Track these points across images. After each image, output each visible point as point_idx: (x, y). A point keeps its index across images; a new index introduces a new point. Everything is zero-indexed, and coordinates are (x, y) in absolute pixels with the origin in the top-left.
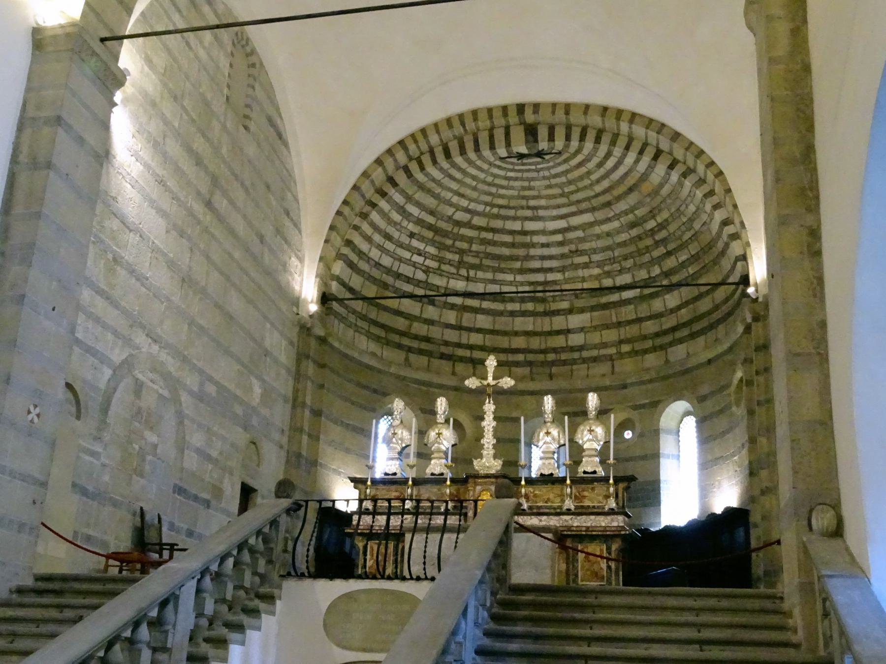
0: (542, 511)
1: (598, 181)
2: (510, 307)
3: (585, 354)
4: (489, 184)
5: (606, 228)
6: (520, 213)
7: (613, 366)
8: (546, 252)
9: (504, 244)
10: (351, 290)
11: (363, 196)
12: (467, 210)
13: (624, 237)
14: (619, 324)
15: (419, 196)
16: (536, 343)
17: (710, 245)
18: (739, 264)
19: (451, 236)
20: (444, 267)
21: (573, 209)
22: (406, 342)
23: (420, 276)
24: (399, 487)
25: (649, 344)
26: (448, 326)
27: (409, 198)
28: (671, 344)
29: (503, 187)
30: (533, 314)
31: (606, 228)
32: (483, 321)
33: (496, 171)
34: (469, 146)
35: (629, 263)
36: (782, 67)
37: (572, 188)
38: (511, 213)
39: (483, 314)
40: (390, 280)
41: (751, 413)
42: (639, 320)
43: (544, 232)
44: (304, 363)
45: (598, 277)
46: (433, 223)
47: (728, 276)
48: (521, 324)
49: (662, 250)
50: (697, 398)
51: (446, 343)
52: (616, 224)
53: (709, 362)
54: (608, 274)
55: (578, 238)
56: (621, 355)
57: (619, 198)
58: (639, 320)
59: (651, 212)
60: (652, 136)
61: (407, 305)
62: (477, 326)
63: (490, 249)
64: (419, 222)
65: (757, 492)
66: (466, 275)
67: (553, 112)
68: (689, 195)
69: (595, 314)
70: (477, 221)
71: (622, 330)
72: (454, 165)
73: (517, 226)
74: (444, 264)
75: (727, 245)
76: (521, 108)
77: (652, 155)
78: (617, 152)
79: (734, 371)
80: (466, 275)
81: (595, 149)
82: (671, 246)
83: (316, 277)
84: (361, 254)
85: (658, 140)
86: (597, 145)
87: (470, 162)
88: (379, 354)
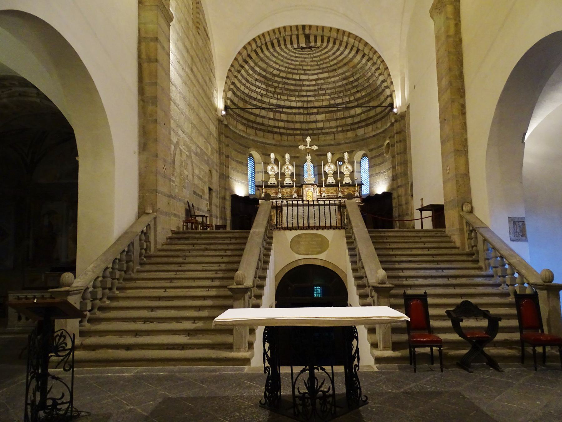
0: (330, 197)
1: (332, 60)
2: (294, 111)
3: (324, 131)
4: (288, 59)
5: (333, 79)
6: (300, 72)
7: (335, 136)
8: (308, 88)
9: (292, 85)
10: (234, 104)
11: (238, 63)
12: (278, 70)
13: (340, 83)
14: (337, 119)
15: (260, 63)
16: (304, 126)
17: (376, 89)
18: (389, 98)
19: (271, 80)
20: (268, 94)
21: (321, 71)
22: (255, 125)
23: (259, 97)
24: (275, 189)
25: (349, 128)
26: (270, 119)
27: (256, 64)
28: (358, 128)
29: (293, 60)
30: (303, 114)
31: (333, 79)
32: (283, 117)
33: (292, 54)
34: (282, 42)
35: (341, 95)
36: (452, 39)
37: (322, 62)
38: (296, 71)
39: (283, 114)
40: (248, 99)
41: (393, 157)
42: (345, 118)
43: (308, 80)
44: (222, 136)
45: (329, 100)
46: (265, 75)
47: (383, 103)
48: (298, 118)
49: (355, 90)
50: (369, 150)
51: (270, 126)
52: (337, 78)
53: (374, 136)
54: (333, 99)
55: (321, 83)
56: (338, 132)
57: (340, 68)
58: (345, 118)
59: (352, 74)
60: (357, 43)
61: (257, 111)
62: (281, 119)
63: (286, 87)
64: (260, 74)
65: (395, 186)
66: (277, 97)
67: (317, 30)
68: (369, 69)
69: (327, 115)
70: (283, 75)
71: (338, 122)
72: (275, 50)
73: (297, 77)
74: (269, 92)
75: (383, 90)
76: (304, 27)
77: (355, 52)
78: (342, 49)
79: (385, 141)
80: (277, 97)
81: (333, 47)
82: (359, 89)
83: (223, 99)
84: (238, 88)
85: (359, 45)
86: (334, 46)
87: (282, 50)
88: (246, 131)
